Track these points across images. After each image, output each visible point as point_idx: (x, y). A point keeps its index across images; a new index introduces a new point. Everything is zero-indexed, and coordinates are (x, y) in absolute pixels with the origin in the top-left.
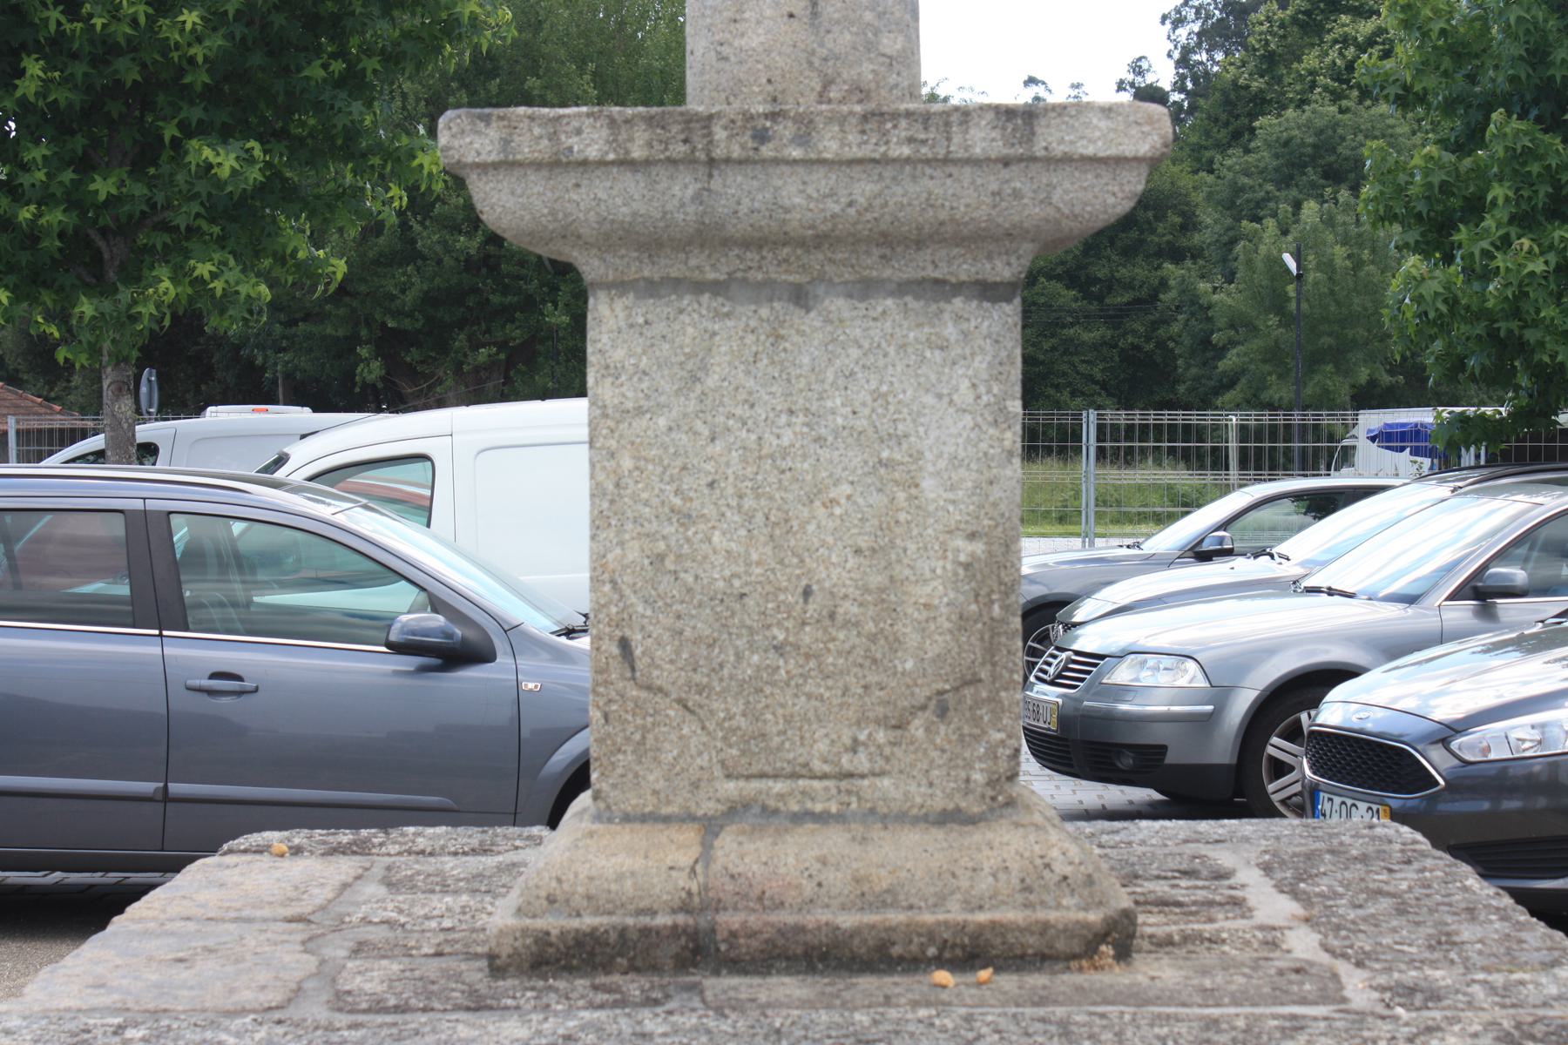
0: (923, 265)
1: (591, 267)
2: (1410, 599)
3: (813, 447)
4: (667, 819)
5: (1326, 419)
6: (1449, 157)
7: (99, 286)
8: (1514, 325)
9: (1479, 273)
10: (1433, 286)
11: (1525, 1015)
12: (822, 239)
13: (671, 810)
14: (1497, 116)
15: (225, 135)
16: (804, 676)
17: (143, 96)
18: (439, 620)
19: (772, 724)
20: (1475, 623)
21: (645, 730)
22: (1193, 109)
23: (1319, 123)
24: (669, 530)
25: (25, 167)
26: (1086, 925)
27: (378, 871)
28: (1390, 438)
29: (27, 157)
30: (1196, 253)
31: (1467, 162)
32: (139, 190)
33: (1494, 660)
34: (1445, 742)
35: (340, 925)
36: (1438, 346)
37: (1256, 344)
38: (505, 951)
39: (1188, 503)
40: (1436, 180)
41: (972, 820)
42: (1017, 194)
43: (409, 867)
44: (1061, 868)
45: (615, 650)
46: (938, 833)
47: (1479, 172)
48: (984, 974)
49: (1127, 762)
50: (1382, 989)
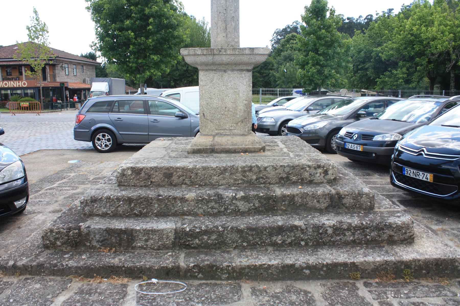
0: (240, 67)
1: (199, 68)
2: (299, 111)
3: (226, 90)
4: (209, 135)
5: (289, 89)
6: (304, 57)
7: (140, 73)
8: (312, 78)
9: (308, 72)
10: (302, 73)
11: (311, 158)
12: (228, 64)
13: (210, 134)
14: (310, 52)
15: (155, 54)
16: (226, 118)
17: (144, 50)
18: (181, 113)
19: (221, 124)
20: (306, 114)
21: (206, 124)
22: (274, 51)
23: (289, 53)
24: (209, 100)
25: (130, 59)
26: (259, 148)
27: (174, 142)
28: (297, 92)
29: (131, 57)
30: (274, 69)
31: (307, 58)
32: (144, 61)
33: (308, 118)
34: (303, 128)
35: (170, 148)
36: (303, 80)
37: (281, 80)
38: (189, 151)
39: (273, 100)
40: (303, 60)
41: (246, 135)
42: (251, 58)
43: (178, 142)
44: (256, 141)
45: (202, 115)
46: (242, 137)
47: (308, 59)
48: (247, 153)
49: (265, 130)
50: (294, 155)
